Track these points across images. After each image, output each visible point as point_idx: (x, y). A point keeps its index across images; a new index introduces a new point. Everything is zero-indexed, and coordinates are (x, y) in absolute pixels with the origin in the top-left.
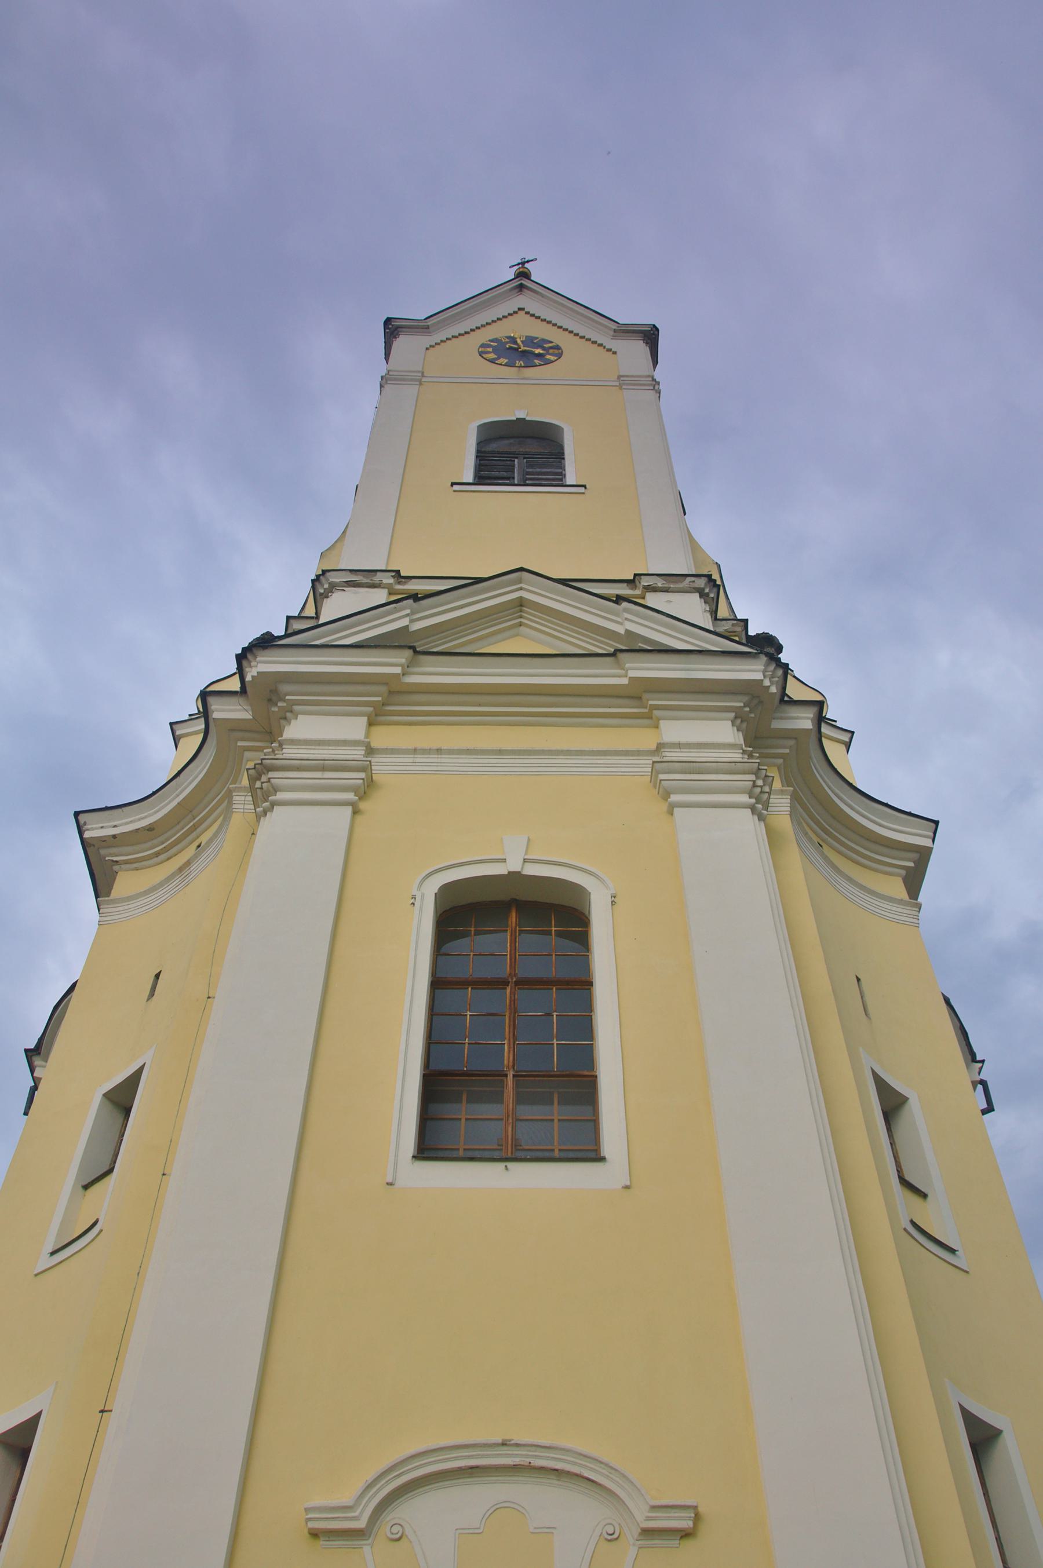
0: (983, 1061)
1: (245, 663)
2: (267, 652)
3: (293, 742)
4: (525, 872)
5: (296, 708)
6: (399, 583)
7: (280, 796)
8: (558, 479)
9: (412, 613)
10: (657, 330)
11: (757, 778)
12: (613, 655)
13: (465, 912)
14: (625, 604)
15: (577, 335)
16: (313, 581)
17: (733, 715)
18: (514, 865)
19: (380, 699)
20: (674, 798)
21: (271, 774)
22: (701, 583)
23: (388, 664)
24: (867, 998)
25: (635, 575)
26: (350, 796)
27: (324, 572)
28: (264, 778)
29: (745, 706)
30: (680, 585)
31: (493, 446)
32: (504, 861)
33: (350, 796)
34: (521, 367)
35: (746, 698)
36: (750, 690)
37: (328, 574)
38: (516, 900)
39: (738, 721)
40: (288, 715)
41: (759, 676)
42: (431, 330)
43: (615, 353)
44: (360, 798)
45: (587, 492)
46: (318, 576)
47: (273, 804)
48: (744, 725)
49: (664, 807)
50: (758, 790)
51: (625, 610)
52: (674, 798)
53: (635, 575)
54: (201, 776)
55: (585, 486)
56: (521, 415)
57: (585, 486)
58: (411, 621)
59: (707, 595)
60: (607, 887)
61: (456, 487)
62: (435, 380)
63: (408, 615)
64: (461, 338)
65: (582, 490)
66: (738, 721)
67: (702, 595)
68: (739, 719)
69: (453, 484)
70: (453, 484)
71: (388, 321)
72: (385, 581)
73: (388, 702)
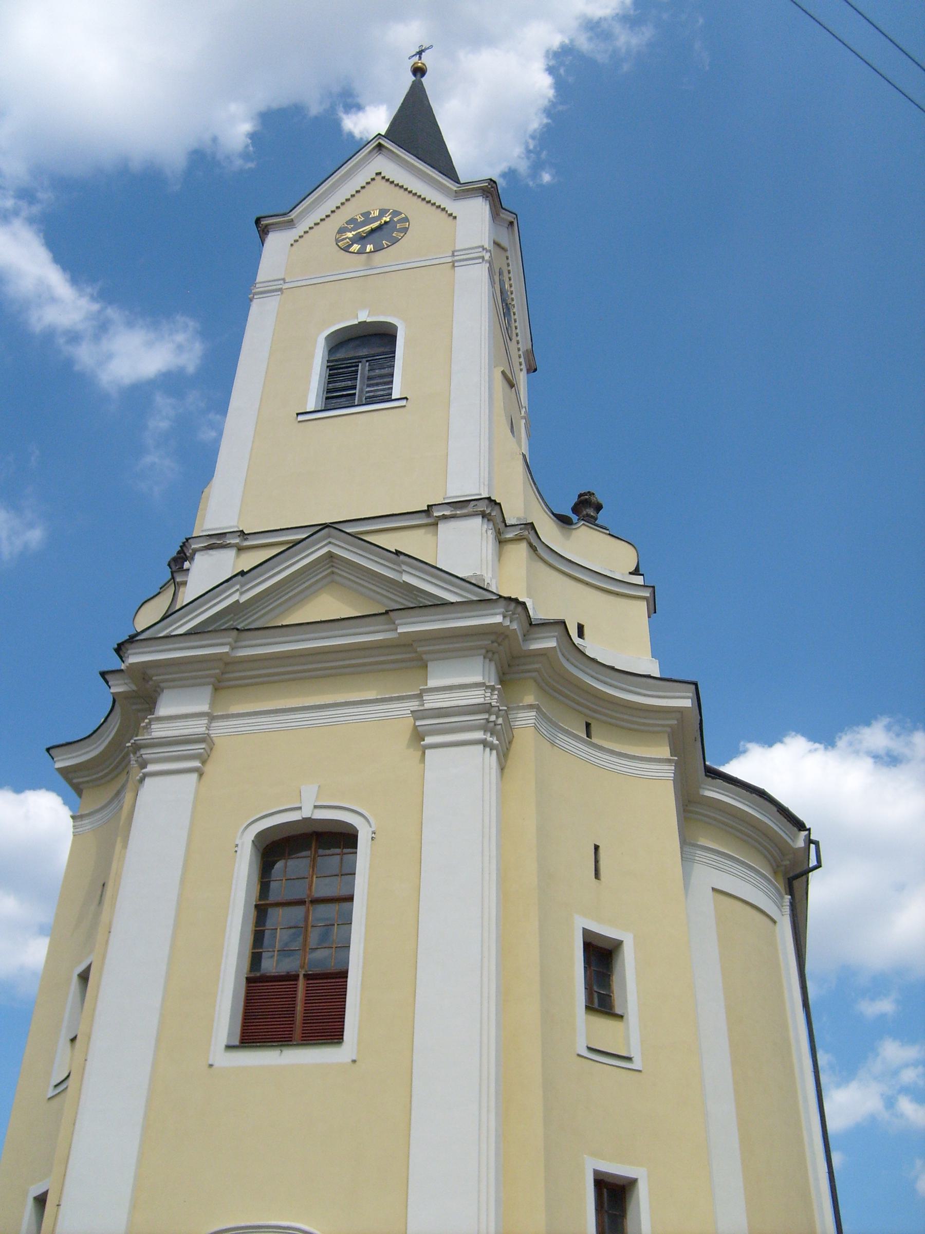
1: (121, 653)
2: (134, 645)
4: (314, 817)
5: (162, 685)
6: (246, 539)
7: (151, 768)
8: (387, 397)
9: (242, 586)
10: (495, 182)
11: (490, 715)
12: (387, 612)
13: (281, 848)
14: (402, 557)
17: (484, 651)
18: (307, 812)
19: (217, 671)
20: (429, 740)
21: (143, 751)
22: (482, 507)
23: (217, 648)
25: (428, 506)
26: (196, 764)
27: (187, 540)
28: (138, 754)
29: (493, 642)
30: (464, 511)
31: (340, 355)
32: (300, 808)
33: (196, 764)
34: (371, 252)
35: (493, 637)
36: (495, 634)
39: (490, 655)
40: (158, 689)
41: (498, 619)
42: (295, 221)
43: (455, 218)
44: (204, 762)
45: (409, 404)
46: (184, 543)
47: (145, 776)
48: (496, 656)
50: (492, 725)
52: (429, 740)
53: (428, 506)
54: (115, 730)
55: (406, 398)
56: (364, 316)
57: (406, 398)
58: (242, 594)
59: (490, 514)
61: (301, 418)
62: (299, 284)
63: (238, 590)
64: (322, 223)
65: (403, 403)
66: (490, 655)
67: (484, 515)
68: (489, 654)
69: (298, 414)
70: (298, 414)
71: (258, 221)
72: (233, 541)
73: (224, 678)
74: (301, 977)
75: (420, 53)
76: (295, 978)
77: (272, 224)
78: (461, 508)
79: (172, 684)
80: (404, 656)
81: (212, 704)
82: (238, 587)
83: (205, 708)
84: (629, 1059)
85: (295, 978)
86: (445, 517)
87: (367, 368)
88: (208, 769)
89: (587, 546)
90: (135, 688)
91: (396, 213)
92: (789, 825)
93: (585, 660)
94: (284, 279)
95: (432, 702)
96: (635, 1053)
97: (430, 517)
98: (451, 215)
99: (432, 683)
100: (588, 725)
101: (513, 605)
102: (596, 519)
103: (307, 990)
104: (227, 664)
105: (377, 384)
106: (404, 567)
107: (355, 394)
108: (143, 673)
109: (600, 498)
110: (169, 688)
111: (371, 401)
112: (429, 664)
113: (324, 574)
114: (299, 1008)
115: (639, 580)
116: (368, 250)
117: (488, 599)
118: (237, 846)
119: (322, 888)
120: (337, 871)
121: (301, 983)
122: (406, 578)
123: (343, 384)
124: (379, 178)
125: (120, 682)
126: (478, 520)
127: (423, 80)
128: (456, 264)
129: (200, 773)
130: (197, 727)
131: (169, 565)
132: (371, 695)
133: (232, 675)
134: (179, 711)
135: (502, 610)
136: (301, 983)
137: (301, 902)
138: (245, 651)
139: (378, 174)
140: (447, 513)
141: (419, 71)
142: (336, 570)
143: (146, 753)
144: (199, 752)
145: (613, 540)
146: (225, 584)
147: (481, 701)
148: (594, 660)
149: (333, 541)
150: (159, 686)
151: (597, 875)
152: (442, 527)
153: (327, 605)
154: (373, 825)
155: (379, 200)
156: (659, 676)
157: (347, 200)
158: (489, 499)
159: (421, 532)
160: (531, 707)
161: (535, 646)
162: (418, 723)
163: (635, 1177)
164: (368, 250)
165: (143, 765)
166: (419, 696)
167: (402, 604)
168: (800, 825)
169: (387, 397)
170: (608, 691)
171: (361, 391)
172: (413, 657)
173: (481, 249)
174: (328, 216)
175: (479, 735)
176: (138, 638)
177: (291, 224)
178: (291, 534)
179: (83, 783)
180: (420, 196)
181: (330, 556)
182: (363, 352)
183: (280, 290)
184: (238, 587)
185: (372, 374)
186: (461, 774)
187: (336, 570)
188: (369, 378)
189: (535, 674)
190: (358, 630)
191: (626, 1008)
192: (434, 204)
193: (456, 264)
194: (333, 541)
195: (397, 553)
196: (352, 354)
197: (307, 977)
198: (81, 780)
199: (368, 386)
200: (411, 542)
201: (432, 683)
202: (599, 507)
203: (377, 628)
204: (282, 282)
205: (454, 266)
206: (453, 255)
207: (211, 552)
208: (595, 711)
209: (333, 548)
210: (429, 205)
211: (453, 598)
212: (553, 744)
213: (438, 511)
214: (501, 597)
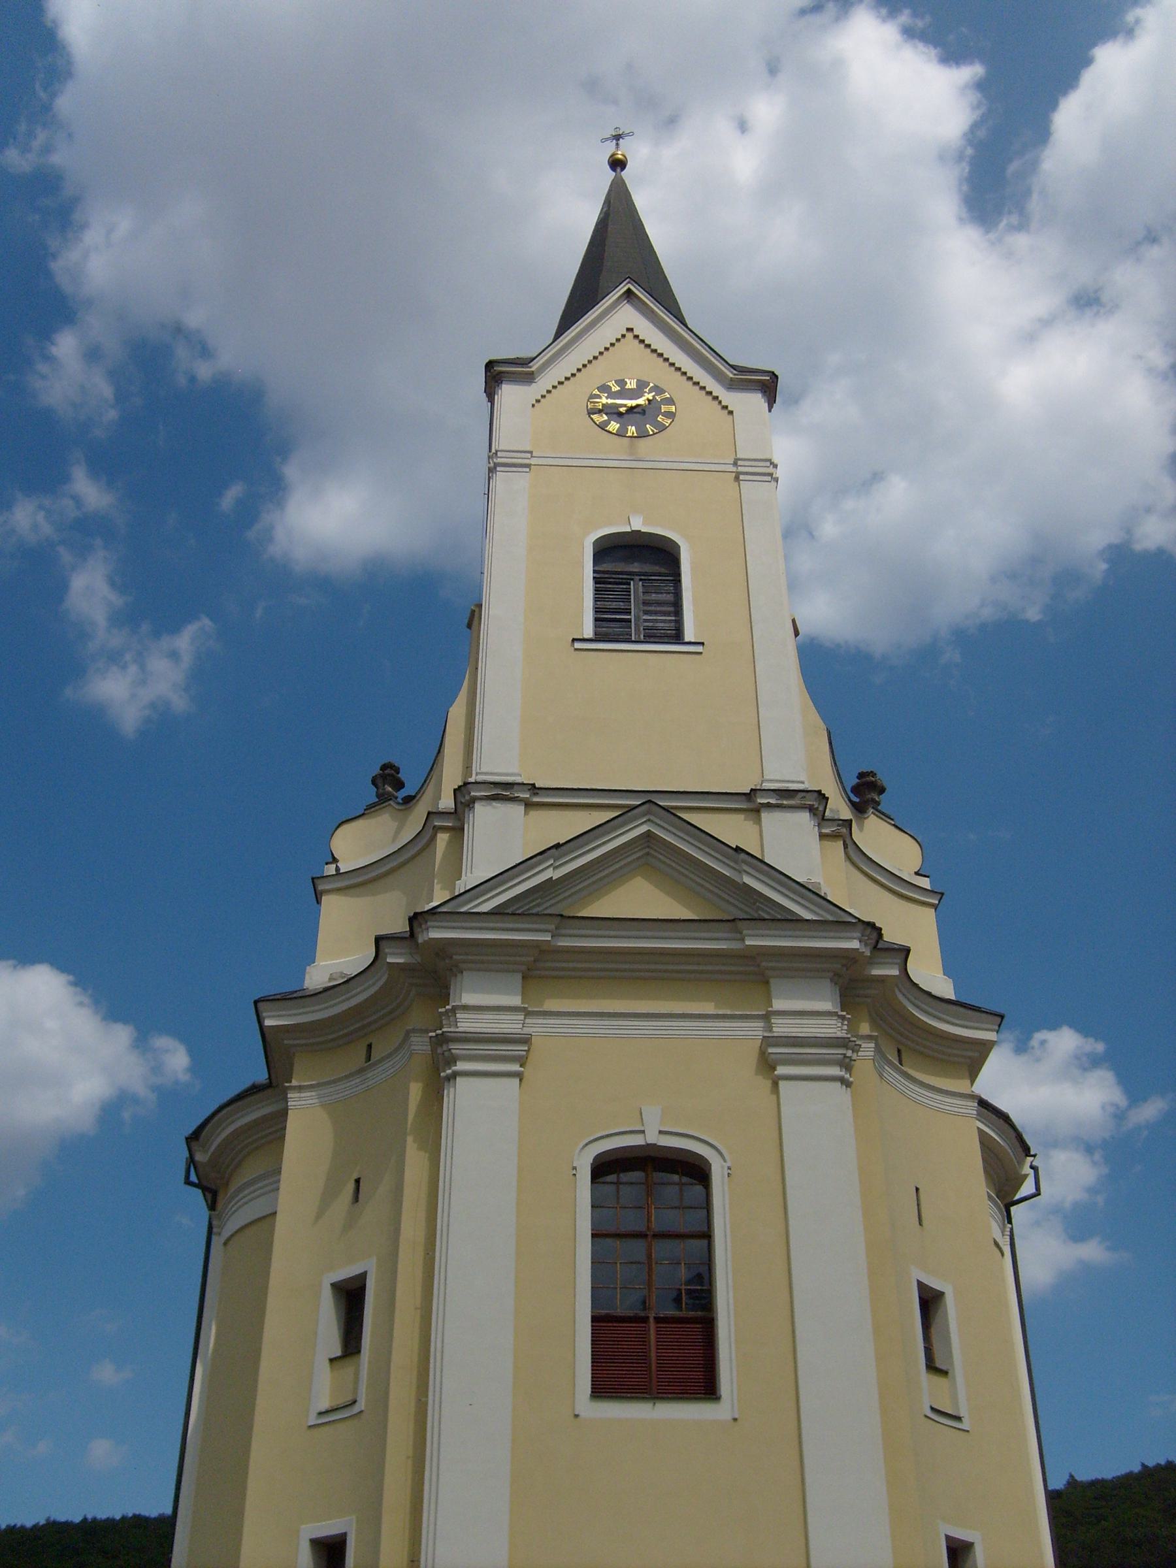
0: (1034, 1156)
1: (415, 924)
3: (466, 1008)
4: (660, 1144)
5: (462, 966)
6: (536, 794)
7: (461, 1066)
10: (777, 377)
12: (734, 920)
14: (743, 856)
15: (690, 378)
16: (455, 790)
18: (652, 1138)
20: (781, 1070)
24: (923, 1210)
26: (516, 1067)
28: (445, 1048)
33: (516, 1067)
36: (848, 957)
37: (469, 786)
38: (650, 1157)
41: (855, 944)
43: (731, 413)
46: (460, 787)
47: (455, 1075)
49: (769, 1083)
51: (744, 862)
52: (781, 1070)
54: (372, 991)
55: (703, 644)
56: (638, 524)
60: (725, 1161)
61: (578, 645)
65: (699, 649)
67: (811, 809)
68: (836, 978)
70: (574, 640)
71: (490, 365)
73: (538, 969)
74: (651, 1320)
75: (617, 137)
76: (645, 1320)
77: (507, 372)
78: (786, 798)
79: (470, 965)
80: (733, 968)
81: (523, 994)
82: (552, 861)
83: (516, 1001)
84: (958, 1418)
85: (645, 1320)
86: (769, 805)
87: (641, 589)
88: (528, 1071)
89: (877, 837)
90: (419, 960)
91: (658, 390)
92: (1017, 1144)
93: (908, 984)
94: (531, 452)
95: (782, 1027)
96: (962, 1413)
97: (752, 803)
98: (725, 407)
99: (778, 1004)
100: (899, 1051)
101: (869, 931)
102: (878, 803)
103: (658, 1332)
104: (542, 952)
105: (656, 613)
106: (745, 868)
107: (629, 621)
108: (443, 949)
109: (883, 778)
110: (470, 969)
111: (652, 636)
112: (772, 981)
113: (635, 856)
114: (653, 1354)
115: (925, 883)
116: (629, 434)
117: (843, 922)
118: (575, 1168)
119: (666, 1219)
120: (677, 1204)
121: (652, 1325)
122: (747, 880)
123: (614, 605)
124: (629, 336)
125: (399, 951)
126: (805, 816)
127: (625, 174)
128: (741, 477)
129: (519, 1076)
130: (510, 1024)
131: (374, 782)
132: (709, 1008)
133: (549, 964)
134: (484, 1003)
135: (859, 935)
136: (652, 1325)
137: (655, 1236)
138: (550, 938)
139: (630, 330)
140: (773, 801)
141: (617, 164)
142: (653, 852)
143: (456, 1048)
144: (514, 1052)
145: (897, 831)
146: (539, 857)
147: (839, 1034)
148: (916, 985)
149: (652, 818)
150: (457, 966)
151: (920, 1224)
152: (765, 816)
153: (640, 898)
154: (727, 1157)
155: (632, 367)
156: (953, 998)
157: (595, 358)
158: (819, 792)
159: (740, 817)
160: (869, 1038)
161: (876, 972)
162: (770, 1050)
163: (971, 1540)
164: (629, 434)
165: (453, 1060)
166: (767, 1017)
167: (746, 912)
168: (1027, 1151)
169: (677, 636)
170: (930, 1022)
171: (637, 618)
172: (753, 974)
173: (768, 464)
174: (573, 375)
175: (835, 1071)
176: (439, 910)
177: (529, 378)
178: (584, 797)
179: (295, 1046)
180: (685, 373)
181: (648, 834)
182: (635, 567)
183: (528, 466)
184: (552, 861)
185: (647, 597)
186: (817, 1112)
187: (653, 852)
188: (645, 603)
189: (869, 1000)
190: (686, 934)
191: (952, 1364)
192: (704, 388)
193: (741, 477)
194: (652, 818)
195: (738, 850)
196: (620, 567)
197: (658, 1320)
198: (291, 1042)
199: (646, 613)
200: (731, 829)
201: (778, 1004)
202: (882, 790)
203: (720, 935)
204: (529, 455)
205: (737, 479)
206: (735, 464)
207: (494, 804)
208: (907, 1038)
209: (653, 827)
210: (648, 350)
211: (808, 916)
212: (881, 1076)
213: (762, 797)
214: (860, 920)
